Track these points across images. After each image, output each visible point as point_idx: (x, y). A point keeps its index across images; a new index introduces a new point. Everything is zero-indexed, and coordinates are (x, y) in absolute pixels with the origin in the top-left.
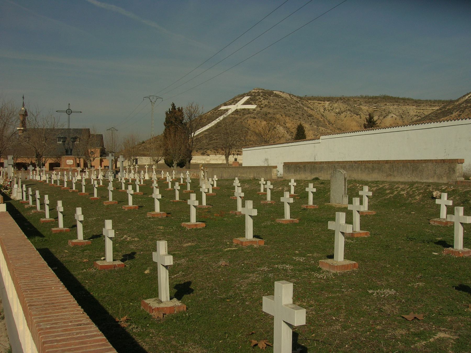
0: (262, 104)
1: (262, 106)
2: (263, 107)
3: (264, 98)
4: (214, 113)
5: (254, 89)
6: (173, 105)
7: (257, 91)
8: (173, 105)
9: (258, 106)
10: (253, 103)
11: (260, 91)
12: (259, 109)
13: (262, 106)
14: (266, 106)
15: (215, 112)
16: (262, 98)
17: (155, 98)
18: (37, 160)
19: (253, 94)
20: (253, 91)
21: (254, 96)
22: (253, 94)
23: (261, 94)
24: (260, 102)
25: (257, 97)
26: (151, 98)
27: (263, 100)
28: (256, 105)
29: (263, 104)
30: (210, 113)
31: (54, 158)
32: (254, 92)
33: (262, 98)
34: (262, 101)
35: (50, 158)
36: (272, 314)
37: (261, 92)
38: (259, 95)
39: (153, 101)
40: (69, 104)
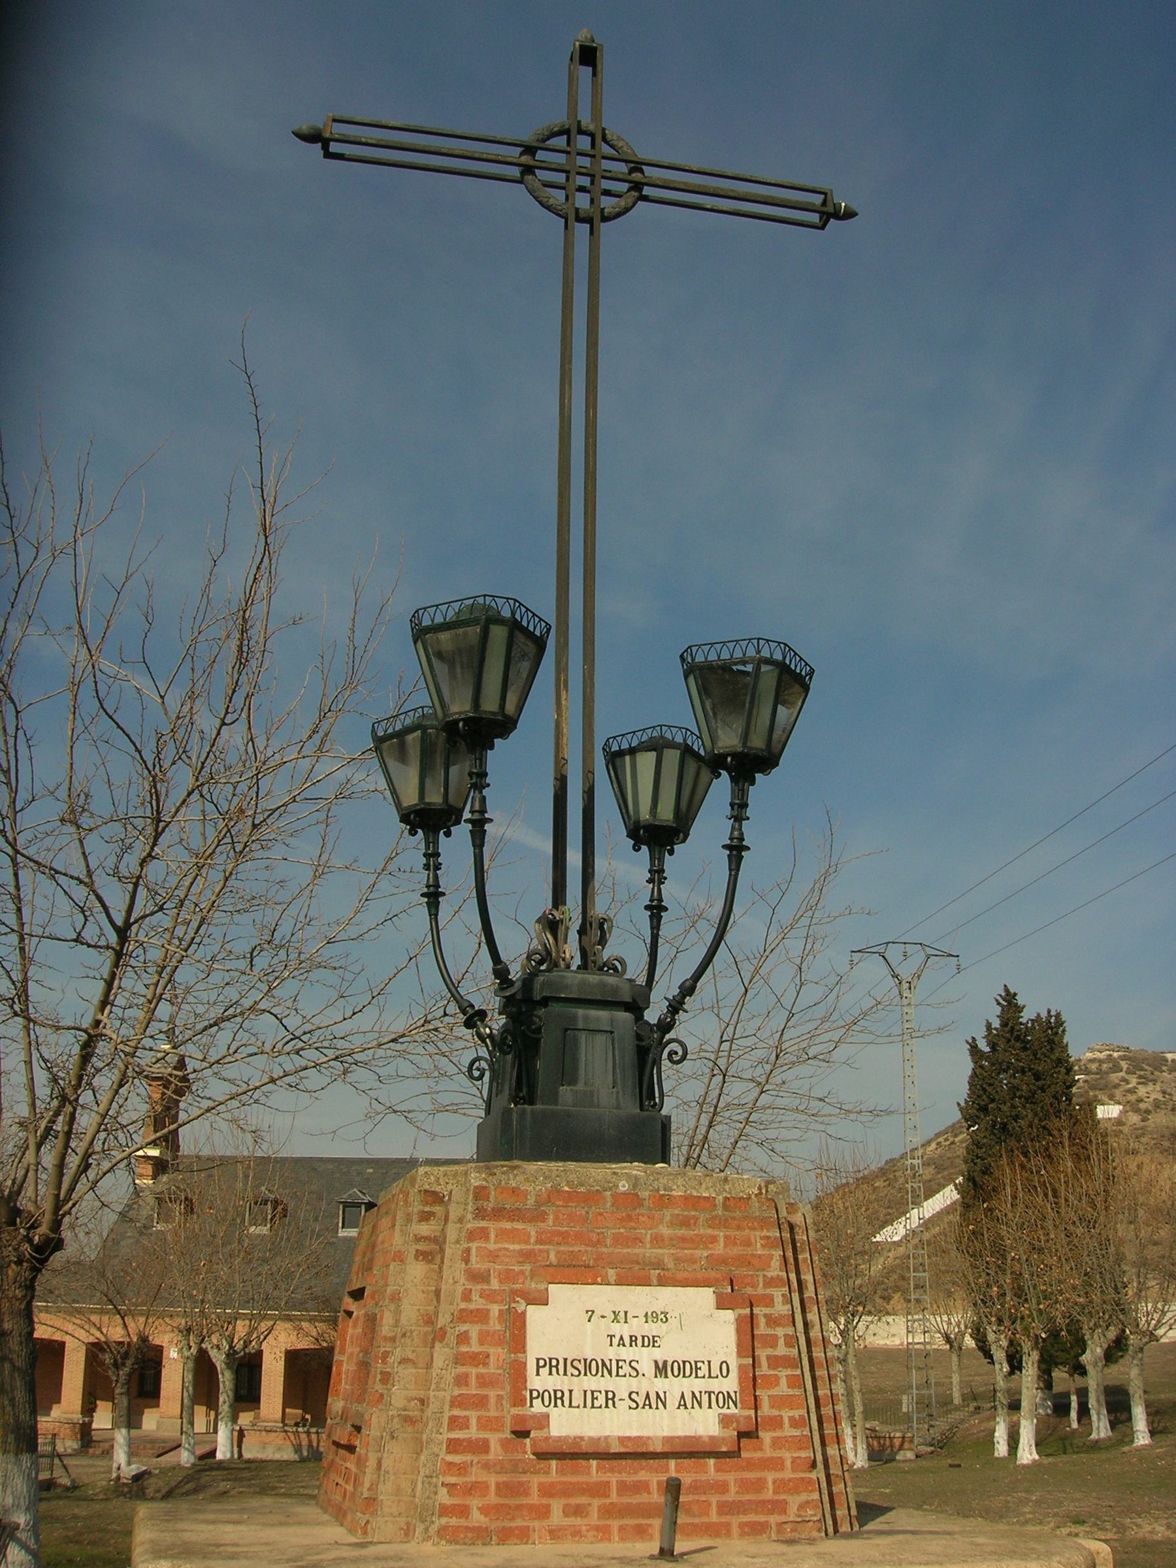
0: (1140, 1100)
1: (1142, 1106)
2: (1148, 1112)
3: (1140, 1077)
4: (953, 1143)
5: (1092, 1050)
6: (1010, 1003)
7: (1102, 1056)
8: (1010, 1003)
9: (1128, 1108)
10: (1106, 1099)
11: (1116, 1054)
12: (1134, 1118)
13: (1142, 1106)
14: (1157, 1105)
15: (956, 1140)
16: (1133, 1081)
17: (918, 957)
18: (189, 1330)
19: (1094, 1067)
20: (1089, 1055)
21: (1097, 1074)
22: (1094, 1067)
23: (1124, 1065)
24: (1132, 1091)
25: (1115, 1077)
26: (894, 953)
27: (1139, 1083)
28: (1120, 1104)
29: (1146, 1100)
30: (933, 1145)
31: (312, 1320)
32: (1092, 1061)
33: (1133, 1081)
34: (1135, 1088)
35: (289, 1319)
36: (162, 1402)
37: (1123, 1058)
38: (1116, 1068)
39: (905, 972)
40: (830, 214)
